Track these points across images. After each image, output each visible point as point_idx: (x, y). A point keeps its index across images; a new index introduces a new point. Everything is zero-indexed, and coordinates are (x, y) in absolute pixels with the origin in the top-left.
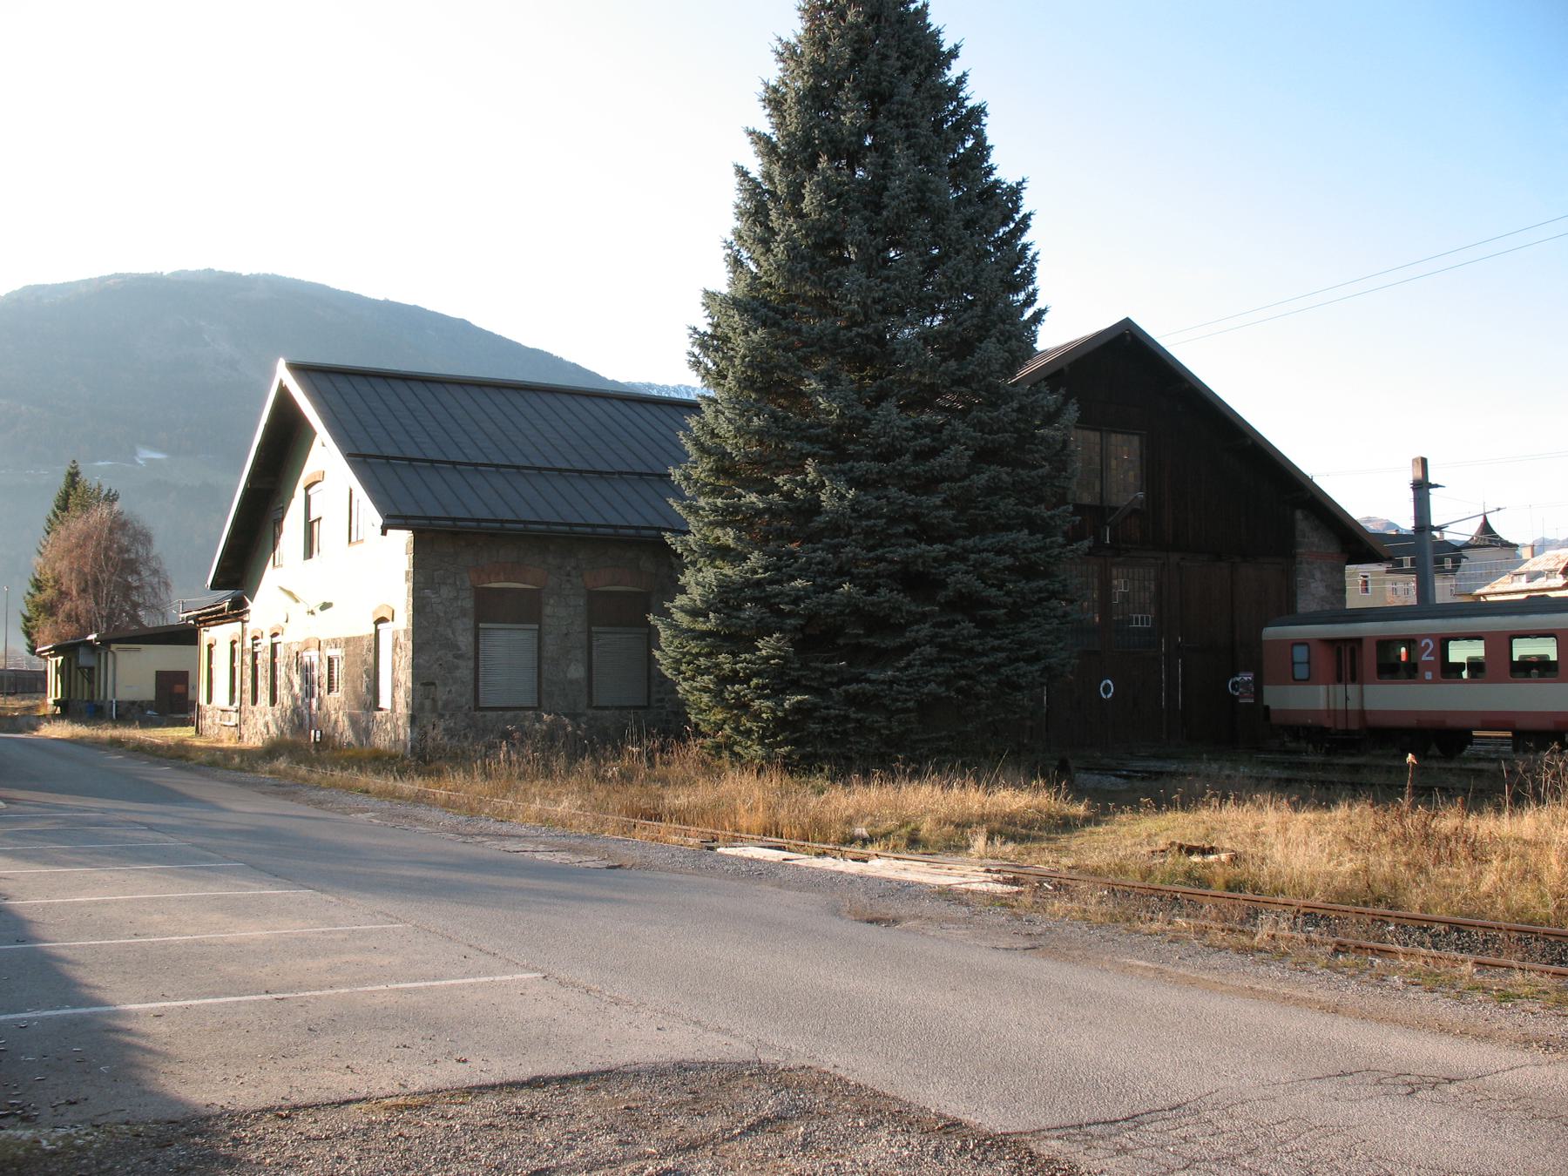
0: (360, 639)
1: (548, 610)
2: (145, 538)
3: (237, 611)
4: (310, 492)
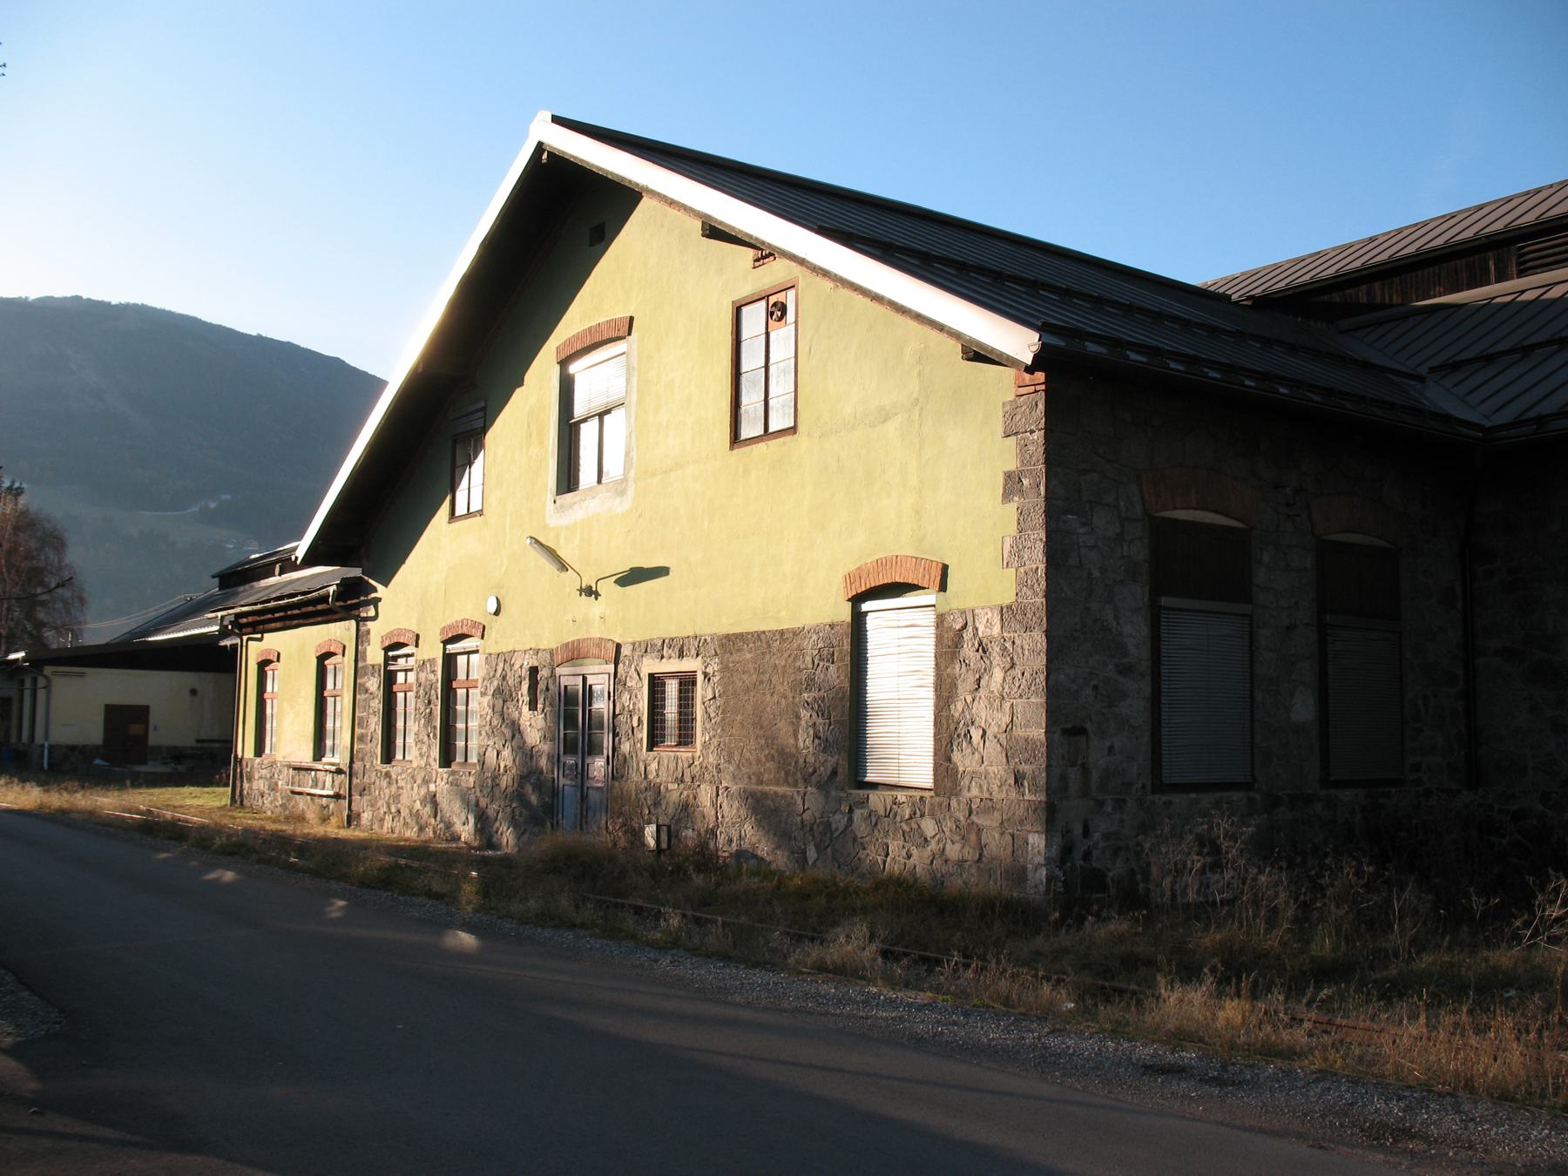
0: (841, 624)
1: (1261, 576)
2: (55, 541)
3: (351, 602)
4: (573, 368)
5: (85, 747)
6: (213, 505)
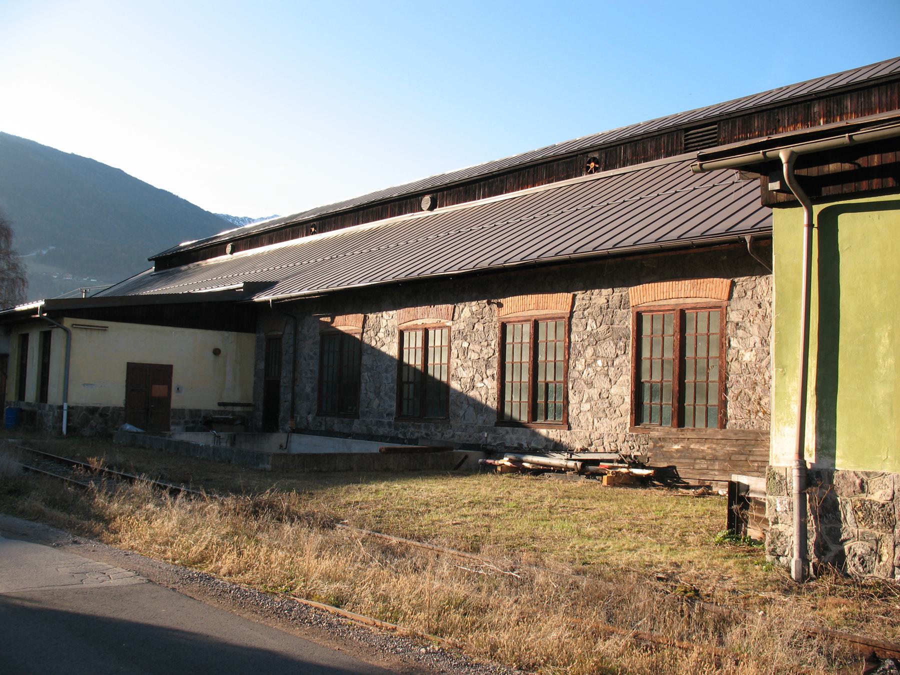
5: (106, 409)
6: (45, 252)
